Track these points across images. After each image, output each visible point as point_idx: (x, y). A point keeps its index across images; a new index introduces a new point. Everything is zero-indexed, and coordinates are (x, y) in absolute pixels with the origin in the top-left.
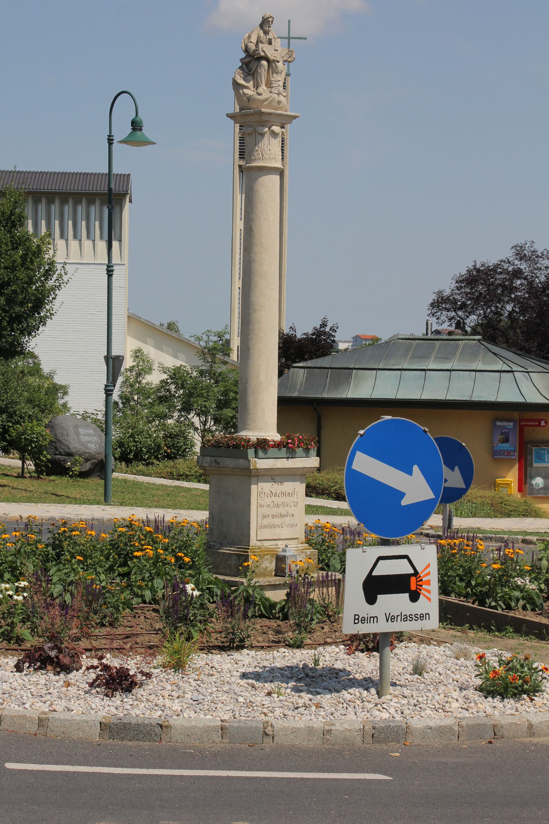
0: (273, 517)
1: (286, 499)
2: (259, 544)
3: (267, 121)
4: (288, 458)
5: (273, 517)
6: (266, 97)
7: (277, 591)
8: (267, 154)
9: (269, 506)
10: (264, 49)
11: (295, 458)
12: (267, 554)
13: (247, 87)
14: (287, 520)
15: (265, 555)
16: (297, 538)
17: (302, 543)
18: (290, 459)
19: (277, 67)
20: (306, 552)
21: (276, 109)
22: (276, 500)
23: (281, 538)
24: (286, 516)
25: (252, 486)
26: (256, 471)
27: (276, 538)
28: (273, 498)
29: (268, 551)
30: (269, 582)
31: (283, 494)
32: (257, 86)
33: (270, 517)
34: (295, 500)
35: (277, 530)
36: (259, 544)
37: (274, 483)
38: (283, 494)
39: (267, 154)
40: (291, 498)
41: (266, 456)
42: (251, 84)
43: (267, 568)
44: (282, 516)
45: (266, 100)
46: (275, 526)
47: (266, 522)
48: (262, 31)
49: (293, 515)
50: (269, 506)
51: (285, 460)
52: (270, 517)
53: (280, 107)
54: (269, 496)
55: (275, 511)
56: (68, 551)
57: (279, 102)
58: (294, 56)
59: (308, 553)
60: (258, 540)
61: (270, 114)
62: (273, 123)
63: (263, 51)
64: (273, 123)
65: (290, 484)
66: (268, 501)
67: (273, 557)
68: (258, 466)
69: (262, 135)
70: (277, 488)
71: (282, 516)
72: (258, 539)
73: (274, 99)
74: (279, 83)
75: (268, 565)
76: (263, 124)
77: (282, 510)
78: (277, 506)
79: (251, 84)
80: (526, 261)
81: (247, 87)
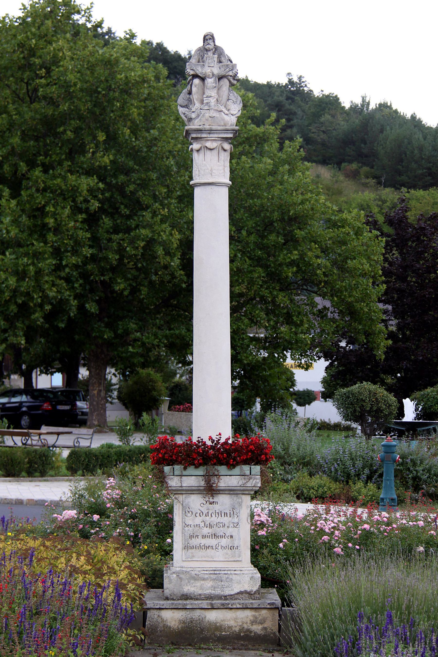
0: (204, 537)
14: (224, 542)
24: (221, 537)
49: (232, 537)
54: (198, 515)
71: (215, 536)
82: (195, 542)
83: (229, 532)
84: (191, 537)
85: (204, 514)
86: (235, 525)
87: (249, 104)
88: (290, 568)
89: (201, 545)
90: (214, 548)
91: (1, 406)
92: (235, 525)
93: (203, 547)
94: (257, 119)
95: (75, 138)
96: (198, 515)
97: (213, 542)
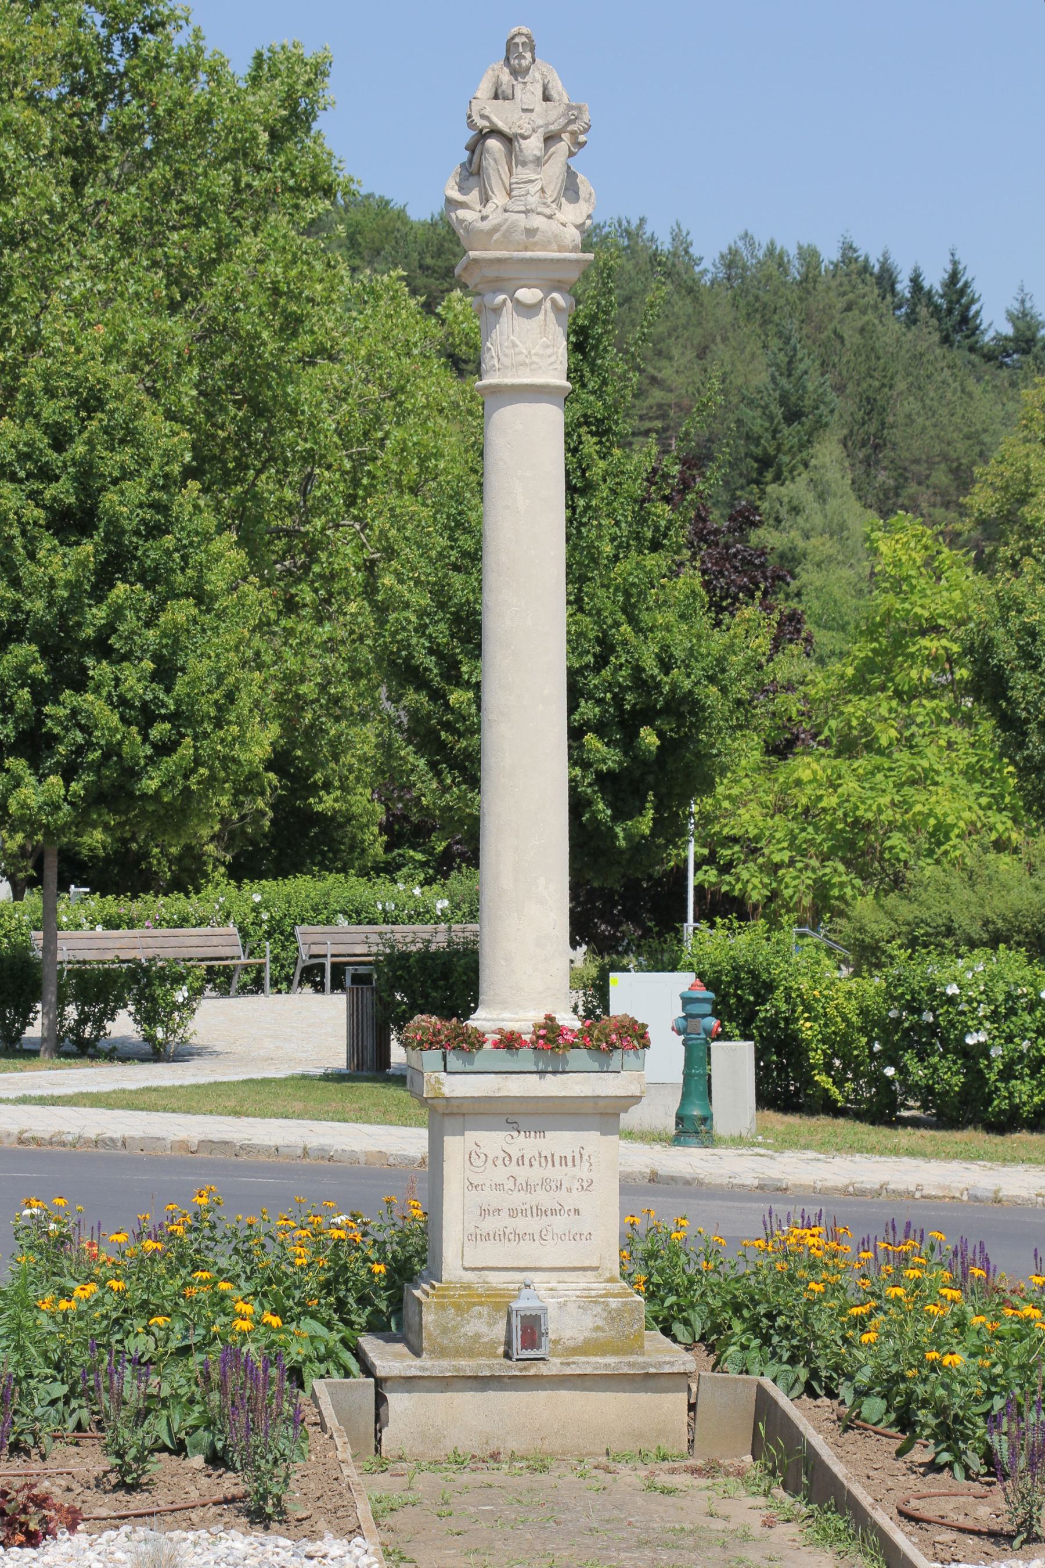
0: (513, 1213)
1: (555, 1173)
2: (470, 1276)
3: (498, 280)
4: (541, 1073)
5: (513, 1213)
6: (495, 222)
7: (491, 1394)
8: (506, 355)
9: (499, 1187)
10: (486, 113)
11: (564, 1072)
12: (481, 1304)
13: (463, 205)
14: (559, 1223)
15: (474, 1304)
16: (596, 1269)
17: (611, 1280)
18: (549, 1075)
19: (521, 150)
20: (607, 1304)
21: (526, 249)
22: (523, 1173)
23: (538, 1265)
24: (554, 1212)
25: (446, 1138)
26: (444, 1102)
27: (522, 1265)
28: (513, 1169)
29: (488, 1296)
30: (458, 1370)
31: (548, 1159)
32: (485, 200)
33: (504, 1214)
34: (585, 1175)
35: (526, 1245)
36: (470, 1276)
37: (515, 1134)
38: (548, 1159)
39: (506, 355)
40: (569, 1170)
41: (469, 1068)
42: (475, 195)
43: (478, 1336)
44: (541, 1212)
45: (495, 229)
46: (519, 1237)
47: (490, 1224)
48: (506, 70)
49: (577, 1212)
50: (499, 1187)
51: (536, 1077)
52: (504, 1214)
53: (535, 244)
54: (499, 1162)
55: (519, 1199)
56: (189, 1274)
57: (531, 232)
58: (586, 117)
59: (614, 1306)
60: (466, 1269)
61: (499, 261)
62: (522, 283)
63: (483, 117)
64: (522, 283)
65: (567, 1135)
66: (500, 1174)
67: (498, 1311)
68: (447, 1091)
69: (497, 311)
70: (524, 1144)
71: (541, 1212)
72: (467, 1265)
73: (512, 228)
74: (529, 186)
75: (484, 1329)
76: (498, 285)
77: (544, 1199)
78: (528, 1187)
79: (475, 195)
80: (376, 577)
81: (463, 205)
82: (490, 1224)
83: (570, 1201)
84: (484, 1212)
85: (514, 1160)
86: (585, 1184)
87: (191, 100)
88: (17, 1400)
89: (507, 1231)
90: (537, 1237)
91: (3, 615)
92: (585, 1184)
93: (512, 1237)
94: (177, 1007)
95: (24, 831)
96: (499, 1162)
97: (533, 1224)
